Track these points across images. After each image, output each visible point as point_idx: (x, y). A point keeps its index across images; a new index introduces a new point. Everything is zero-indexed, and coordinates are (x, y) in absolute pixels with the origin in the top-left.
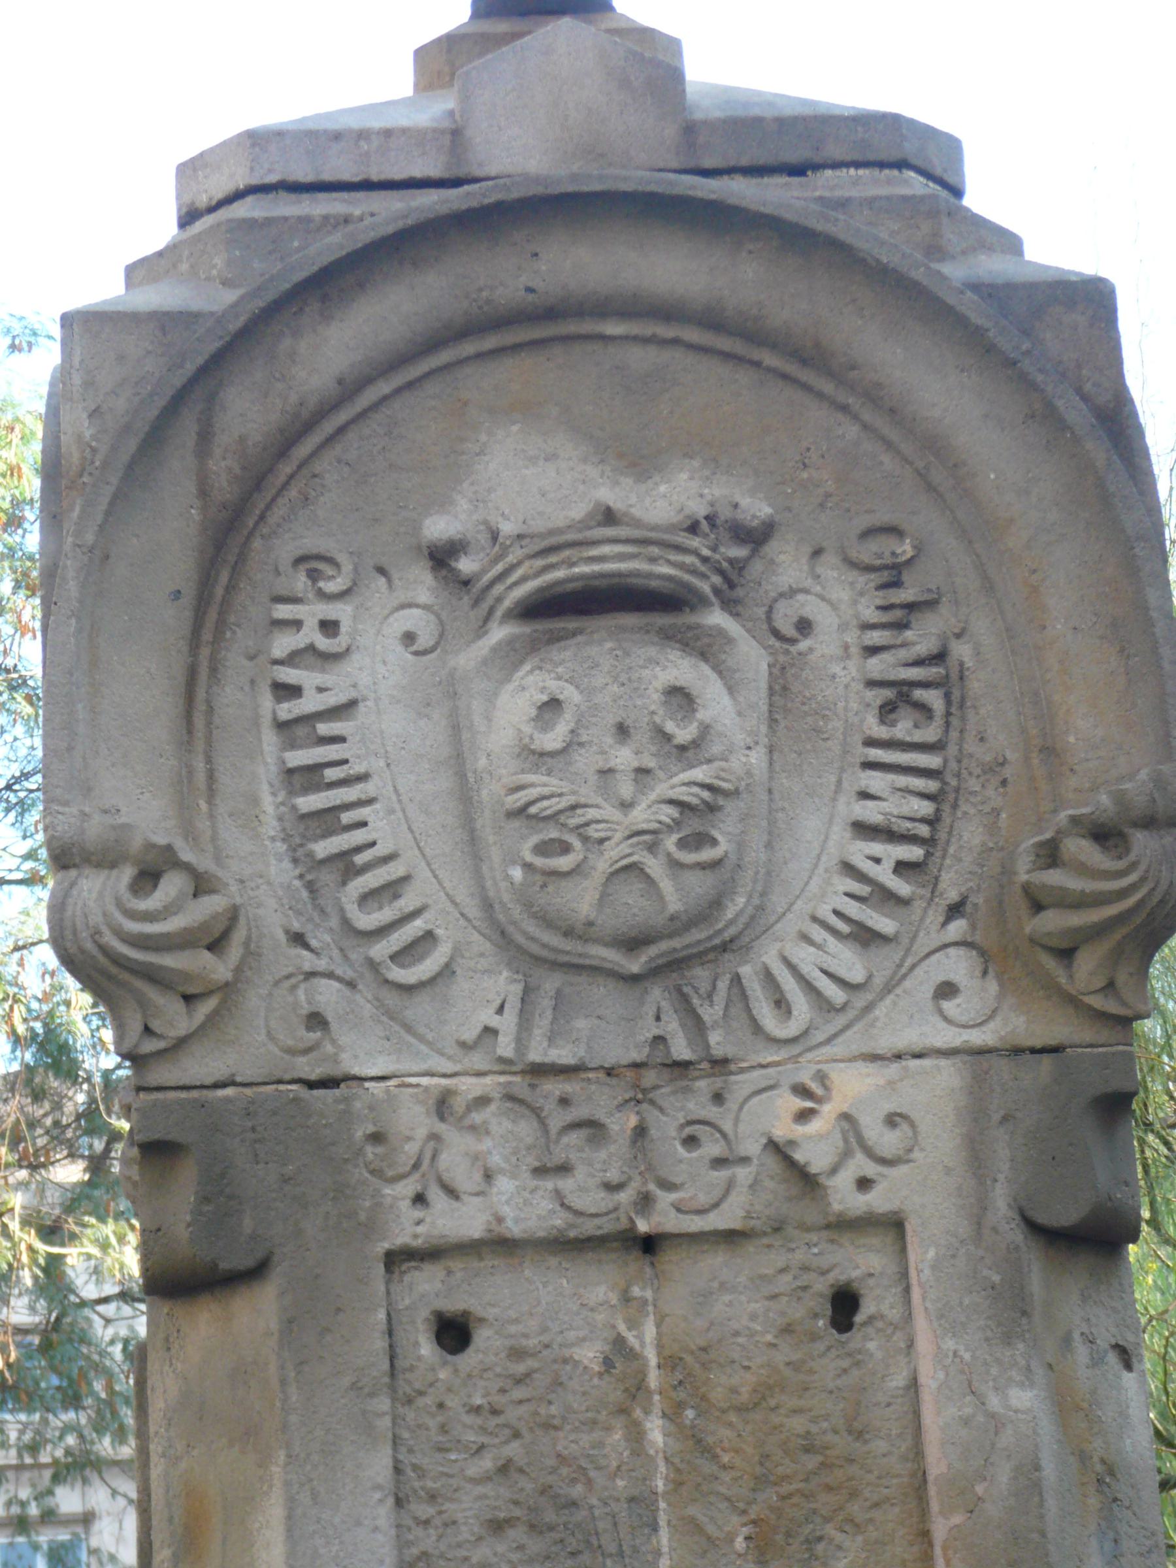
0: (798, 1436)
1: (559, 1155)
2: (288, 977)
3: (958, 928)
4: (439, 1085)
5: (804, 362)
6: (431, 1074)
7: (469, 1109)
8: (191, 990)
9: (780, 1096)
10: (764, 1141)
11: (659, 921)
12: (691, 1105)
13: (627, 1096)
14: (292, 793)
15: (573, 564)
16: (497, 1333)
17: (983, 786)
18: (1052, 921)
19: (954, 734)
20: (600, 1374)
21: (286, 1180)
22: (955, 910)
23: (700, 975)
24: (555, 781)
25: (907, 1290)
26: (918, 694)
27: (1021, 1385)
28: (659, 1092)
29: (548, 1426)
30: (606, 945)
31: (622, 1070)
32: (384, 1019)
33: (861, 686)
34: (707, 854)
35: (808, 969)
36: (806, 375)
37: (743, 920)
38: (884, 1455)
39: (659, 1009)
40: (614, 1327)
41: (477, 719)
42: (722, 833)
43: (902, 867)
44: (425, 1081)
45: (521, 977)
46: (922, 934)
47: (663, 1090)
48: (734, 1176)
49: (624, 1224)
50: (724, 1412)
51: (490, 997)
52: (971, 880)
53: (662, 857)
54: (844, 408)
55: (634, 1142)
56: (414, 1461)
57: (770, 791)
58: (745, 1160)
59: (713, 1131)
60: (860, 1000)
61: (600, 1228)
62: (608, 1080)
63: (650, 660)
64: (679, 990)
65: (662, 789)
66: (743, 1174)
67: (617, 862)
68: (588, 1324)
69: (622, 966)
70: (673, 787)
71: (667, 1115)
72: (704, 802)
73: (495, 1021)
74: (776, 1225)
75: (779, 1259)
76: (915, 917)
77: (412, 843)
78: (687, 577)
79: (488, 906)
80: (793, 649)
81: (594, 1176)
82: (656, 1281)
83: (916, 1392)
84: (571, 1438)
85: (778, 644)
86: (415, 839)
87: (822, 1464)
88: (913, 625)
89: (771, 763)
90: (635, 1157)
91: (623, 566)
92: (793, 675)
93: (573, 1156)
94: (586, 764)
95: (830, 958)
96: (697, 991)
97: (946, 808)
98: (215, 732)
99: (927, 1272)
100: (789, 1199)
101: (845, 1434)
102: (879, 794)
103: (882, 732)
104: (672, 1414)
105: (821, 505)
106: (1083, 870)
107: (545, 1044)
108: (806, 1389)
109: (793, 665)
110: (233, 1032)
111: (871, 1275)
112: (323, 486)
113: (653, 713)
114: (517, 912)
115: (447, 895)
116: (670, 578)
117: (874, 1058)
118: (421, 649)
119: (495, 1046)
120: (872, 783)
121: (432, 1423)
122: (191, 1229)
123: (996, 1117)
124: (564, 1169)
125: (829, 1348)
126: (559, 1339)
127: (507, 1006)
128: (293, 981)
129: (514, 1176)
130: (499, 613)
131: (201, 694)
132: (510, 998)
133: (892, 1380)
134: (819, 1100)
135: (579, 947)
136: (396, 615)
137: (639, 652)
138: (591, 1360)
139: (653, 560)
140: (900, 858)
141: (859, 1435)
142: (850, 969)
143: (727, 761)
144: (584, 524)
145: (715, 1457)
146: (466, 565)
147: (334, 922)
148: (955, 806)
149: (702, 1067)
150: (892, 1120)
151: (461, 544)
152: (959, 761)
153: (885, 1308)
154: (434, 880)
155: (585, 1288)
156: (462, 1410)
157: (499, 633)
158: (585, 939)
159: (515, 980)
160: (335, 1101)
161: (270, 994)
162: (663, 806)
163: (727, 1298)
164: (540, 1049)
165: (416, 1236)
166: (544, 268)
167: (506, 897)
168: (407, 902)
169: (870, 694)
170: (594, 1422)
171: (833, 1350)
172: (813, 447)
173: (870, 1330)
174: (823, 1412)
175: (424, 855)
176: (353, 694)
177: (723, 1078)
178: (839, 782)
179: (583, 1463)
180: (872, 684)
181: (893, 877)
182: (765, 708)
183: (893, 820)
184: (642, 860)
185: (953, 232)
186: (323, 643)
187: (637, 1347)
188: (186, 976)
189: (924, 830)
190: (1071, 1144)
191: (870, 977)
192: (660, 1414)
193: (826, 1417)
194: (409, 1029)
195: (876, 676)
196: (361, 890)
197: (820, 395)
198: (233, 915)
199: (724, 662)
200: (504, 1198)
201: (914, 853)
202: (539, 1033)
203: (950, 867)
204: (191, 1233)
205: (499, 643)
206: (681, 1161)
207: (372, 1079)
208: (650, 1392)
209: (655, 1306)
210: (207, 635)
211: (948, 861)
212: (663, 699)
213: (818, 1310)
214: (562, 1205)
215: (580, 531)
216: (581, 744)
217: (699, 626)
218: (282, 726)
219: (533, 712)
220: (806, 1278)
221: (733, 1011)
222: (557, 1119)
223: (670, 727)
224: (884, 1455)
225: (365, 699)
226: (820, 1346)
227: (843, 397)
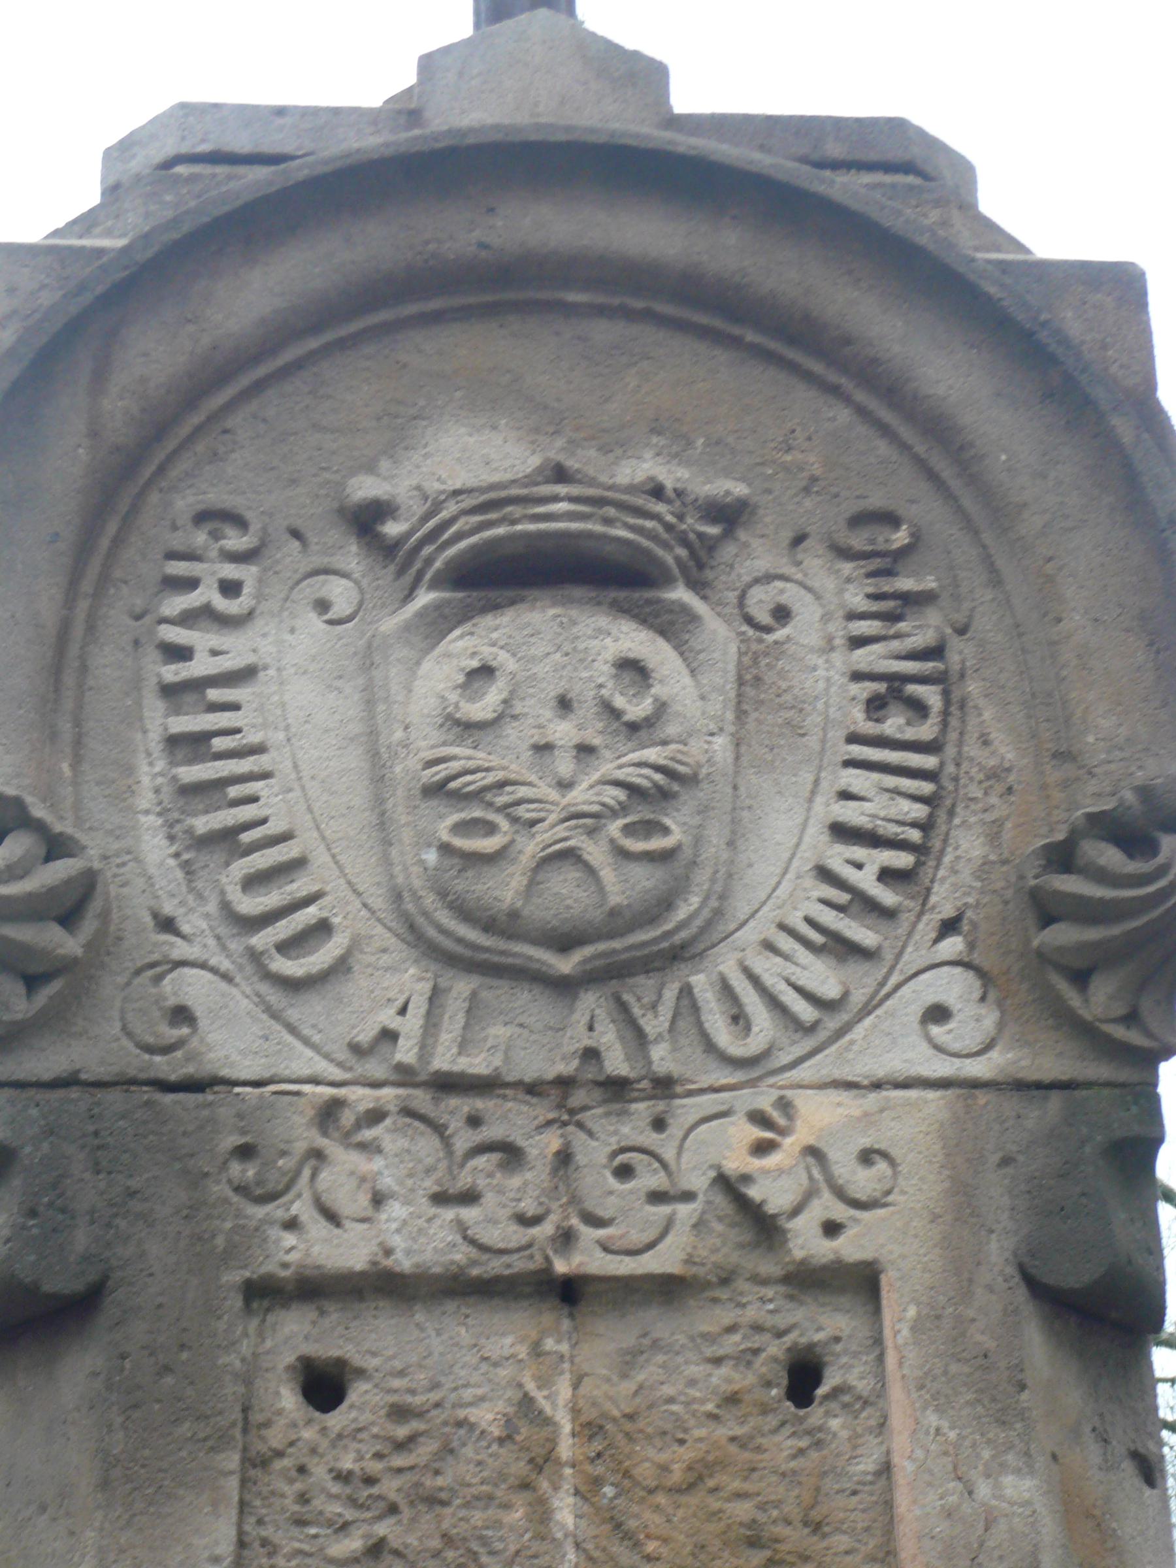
0: (741, 1524)
1: (464, 1180)
3: (953, 945)
4: (321, 1095)
5: (793, 340)
6: (315, 1081)
7: (358, 1126)
8: (34, 968)
9: (733, 1124)
10: (712, 1174)
11: (597, 915)
12: (626, 1130)
14: (173, 763)
15: (514, 522)
18: (1063, 935)
19: (953, 736)
20: (501, 1441)
22: (949, 927)
23: (645, 984)
24: (481, 755)
25: (881, 1359)
26: (914, 689)
27: (1018, 1471)
28: (589, 1113)
29: (434, 1501)
31: (546, 1087)
32: (264, 1017)
33: (845, 680)
34: (656, 843)
35: (769, 980)
37: (699, 922)
38: (847, 1553)
39: (592, 1017)
40: (520, 1385)
41: (394, 688)
42: (676, 823)
43: (887, 875)
44: (307, 1088)
46: (909, 949)
47: (593, 1111)
48: (674, 1213)
49: (537, 1263)
50: (651, 1491)
51: (391, 995)
53: (604, 846)
54: (834, 390)
55: (555, 1171)
56: (264, 1533)
57: (735, 788)
58: (688, 1196)
59: (653, 1160)
60: (832, 1023)
61: (509, 1266)
62: (528, 1097)
65: (606, 767)
66: (684, 1211)
67: (550, 845)
68: (490, 1381)
69: (550, 966)
70: (620, 767)
72: (656, 785)
73: (395, 1023)
74: (724, 1275)
75: (727, 1316)
76: (902, 931)
77: (311, 824)
78: (645, 543)
79: (397, 897)
80: (770, 638)
81: (504, 1206)
83: (889, 1478)
84: (461, 1515)
85: (751, 632)
87: (770, 1560)
89: (737, 758)
90: (556, 1188)
91: (575, 526)
93: (482, 1183)
95: (798, 970)
96: (639, 999)
97: (942, 815)
99: (905, 1332)
100: (741, 1246)
101: (800, 1525)
102: (862, 794)
103: (869, 728)
104: (588, 1491)
106: (1102, 876)
107: (455, 1050)
108: (754, 1470)
109: (766, 654)
111: (837, 1339)
113: (601, 686)
114: (430, 900)
115: (349, 883)
117: (850, 1085)
118: (335, 617)
119: (393, 1053)
121: (291, 1490)
122: (9, 1245)
123: (995, 1158)
124: (469, 1197)
125: (783, 1424)
126: (453, 1397)
127: (411, 1006)
128: (159, 970)
129: (407, 1202)
131: (74, 650)
133: (858, 1464)
134: (783, 1132)
135: (502, 944)
138: (490, 1424)
139: (608, 521)
140: (886, 864)
141: (817, 1528)
142: (823, 982)
143: (685, 745)
145: (637, 1544)
146: (392, 529)
147: (212, 907)
148: (951, 813)
149: (640, 1086)
150: (867, 1157)
152: (958, 765)
153: (853, 1379)
155: (488, 1338)
156: (328, 1477)
157: (425, 598)
158: (511, 936)
161: (128, 984)
162: (608, 787)
165: (285, 1266)
166: (500, 223)
168: (300, 886)
169: (855, 688)
170: (490, 1497)
171: (788, 1426)
172: (799, 429)
173: (834, 1406)
174: (773, 1497)
176: (250, 659)
178: (817, 782)
179: (475, 1546)
180: (858, 676)
181: (877, 884)
183: (879, 822)
184: (579, 844)
186: (221, 603)
187: (548, 1410)
188: (26, 950)
190: (1084, 1194)
191: (846, 995)
192: (572, 1491)
193: (777, 1504)
194: (292, 1030)
195: (863, 667)
198: (88, 884)
199: (687, 642)
200: (394, 1226)
202: (448, 1037)
203: (943, 879)
204: (10, 1249)
206: (611, 1193)
207: (245, 1083)
208: (559, 1464)
209: (572, 1362)
210: (87, 586)
211: (941, 873)
212: (613, 671)
213: (770, 1377)
214: (465, 1238)
215: (526, 486)
216: (515, 717)
217: (659, 601)
220: (757, 1341)
221: (682, 1024)
222: (464, 1140)
223: (619, 702)
224: (847, 1553)
225: (265, 668)
226: (772, 1421)
227: (833, 377)
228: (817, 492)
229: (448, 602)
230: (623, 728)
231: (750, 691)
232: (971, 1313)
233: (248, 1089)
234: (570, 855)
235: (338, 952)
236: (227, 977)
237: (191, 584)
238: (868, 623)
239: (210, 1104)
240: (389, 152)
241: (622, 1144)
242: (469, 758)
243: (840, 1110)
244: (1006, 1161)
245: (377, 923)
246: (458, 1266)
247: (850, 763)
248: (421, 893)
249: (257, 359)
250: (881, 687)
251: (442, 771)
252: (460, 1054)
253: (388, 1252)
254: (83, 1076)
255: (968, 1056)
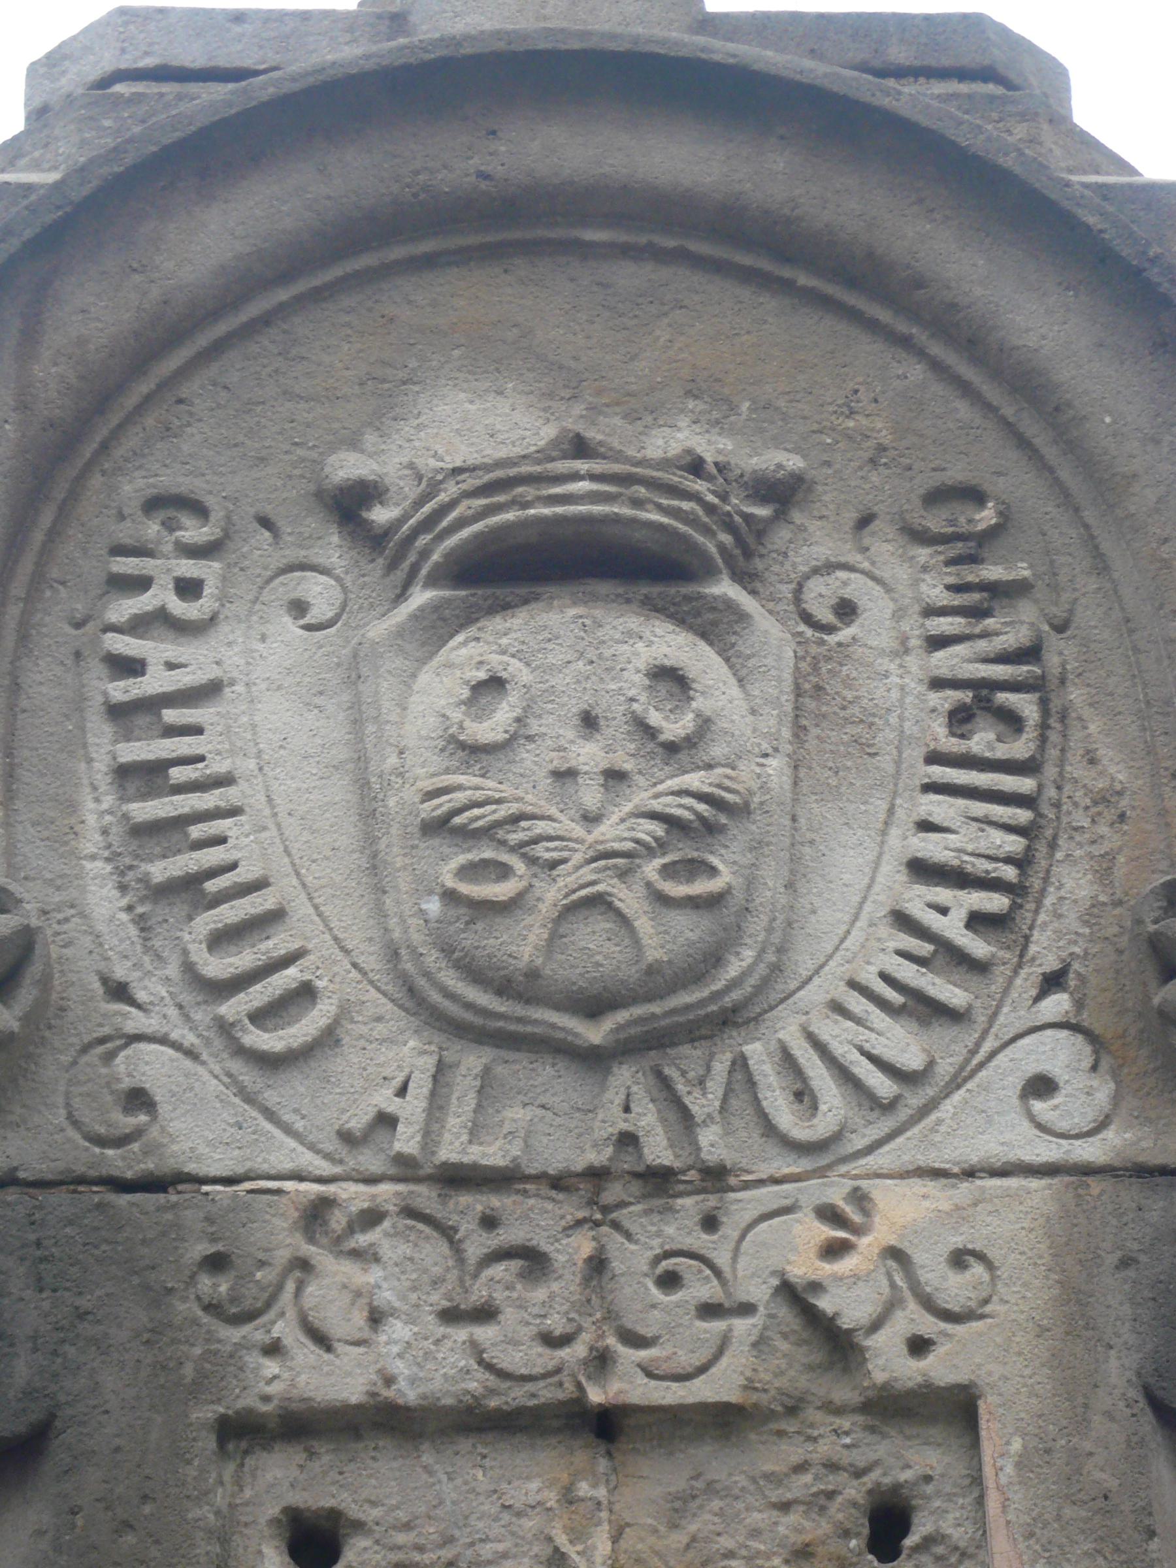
1: (479, 1293)
2: (102, 1041)
3: (1057, 1004)
5: (853, 283)
6: (299, 1177)
7: (351, 1230)
10: (775, 1282)
12: (670, 1230)
13: (580, 1214)
14: (124, 799)
15: (525, 505)
16: (377, 1542)
17: (1093, 821)
19: (1053, 753)
21: (82, 1315)
22: (1052, 982)
23: (690, 1054)
24: (490, 784)
25: (980, 1501)
26: (1003, 698)
28: (625, 1211)
30: (557, 1007)
31: (574, 1180)
33: (922, 688)
34: (701, 887)
35: (839, 1049)
36: (852, 299)
37: (753, 980)
40: (550, 1539)
42: (724, 862)
43: (977, 921)
44: (289, 1185)
45: (433, 1048)
47: (632, 1208)
48: (730, 1329)
51: (387, 1072)
52: (1075, 942)
53: (641, 891)
54: (904, 342)
55: (587, 1280)
57: (794, 819)
58: (747, 1309)
59: (703, 1267)
60: (915, 1100)
61: (533, 1395)
62: (553, 1193)
63: (630, 634)
64: (659, 1075)
65: (641, 797)
66: (741, 1326)
67: (574, 891)
68: (513, 1534)
69: (576, 1035)
70: (657, 796)
71: (636, 1242)
73: (393, 1105)
74: (790, 1403)
77: (290, 870)
79: (393, 954)
80: (832, 639)
81: (528, 1324)
82: (613, 1477)
85: (809, 632)
86: (293, 864)
88: (996, 613)
89: (795, 783)
90: (589, 1301)
92: (830, 671)
93: (499, 1295)
94: (536, 763)
95: (874, 1036)
96: (684, 1073)
97: (1042, 848)
98: (20, 716)
99: (1009, 1469)
100: (810, 1368)
102: (945, 824)
103: (953, 745)
105: (873, 461)
107: (465, 1138)
110: (19, 1110)
111: (928, 1479)
112: (191, 414)
113: (632, 700)
114: (432, 958)
115: (336, 939)
116: (661, 527)
118: (313, 621)
119: (391, 1142)
120: (935, 809)
123: (1112, 1259)
124: (485, 1314)
129: (411, 1321)
130: (424, 572)
132: (416, 1075)
134: (858, 1231)
135: (519, 1010)
136: (281, 579)
137: (615, 623)
140: (975, 908)
143: (733, 769)
144: (544, 456)
147: (173, 970)
148: (1053, 846)
150: (959, 1259)
151: (376, 487)
153: (947, 1527)
154: (316, 919)
157: (420, 597)
159: (425, 1052)
160: (158, 1210)
163: (716, 1504)
164: (457, 1144)
167: (416, 938)
168: (277, 943)
172: (862, 389)
175: (304, 885)
176: (213, 673)
177: (719, 1195)
178: (891, 811)
180: (938, 684)
181: (965, 932)
182: (789, 708)
183: (966, 858)
184: (609, 889)
185: (1055, 143)
186: (178, 607)
189: (1009, 873)
191: (931, 1064)
194: (270, 1114)
195: (944, 672)
196: (213, 926)
197: (872, 326)
199: (733, 645)
200: (395, 1349)
201: (996, 902)
202: (456, 1121)
205: (421, 609)
211: (1042, 917)
212: (647, 682)
214: (481, 1362)
216: (530, 738)
217: (701, 597)
218: (118, 712)
219: (466, 693)
220: (832, 1481)
221: (734, 1103)
222: (477, 1245)
223: (655, 718)
225: (232, 683)
228: (885, 464)
229: (448, 601)
230: (660, 750)
231: (809, 704)
232: (1088, 1446)
233: (219, 1188)
234: (599, 902)
235: (323, 1022)
236: (191, 1054)
237: (142, 584)
238: (949, 619)
239: (174, 1206)
240: (370, 65)
241: (667, 1247)
242: (477, 788)
243: (926, 1204)
244: (1126, 1262)
245: (369, 987)
246: (473, 1396)
247: (932, 788)
248: (421, 950)
249: (215, 314)
250: (967, 696)
251: (444, 804)
252: (470, 1142)
253: (389, 1381)
254: (22, 1175)
255: (1077, 1136)
